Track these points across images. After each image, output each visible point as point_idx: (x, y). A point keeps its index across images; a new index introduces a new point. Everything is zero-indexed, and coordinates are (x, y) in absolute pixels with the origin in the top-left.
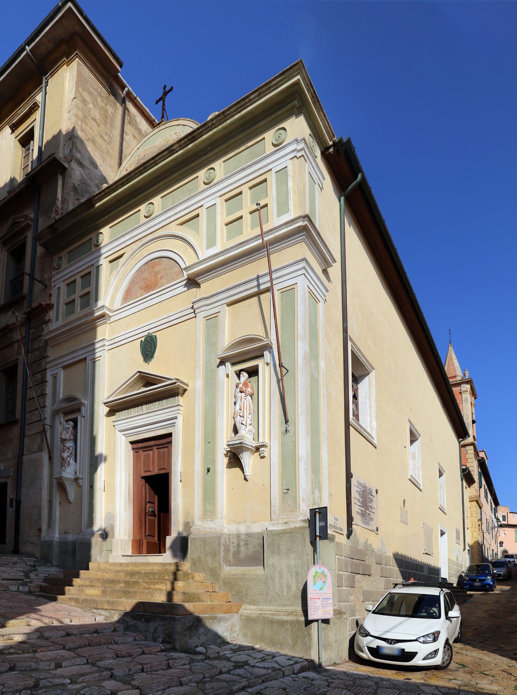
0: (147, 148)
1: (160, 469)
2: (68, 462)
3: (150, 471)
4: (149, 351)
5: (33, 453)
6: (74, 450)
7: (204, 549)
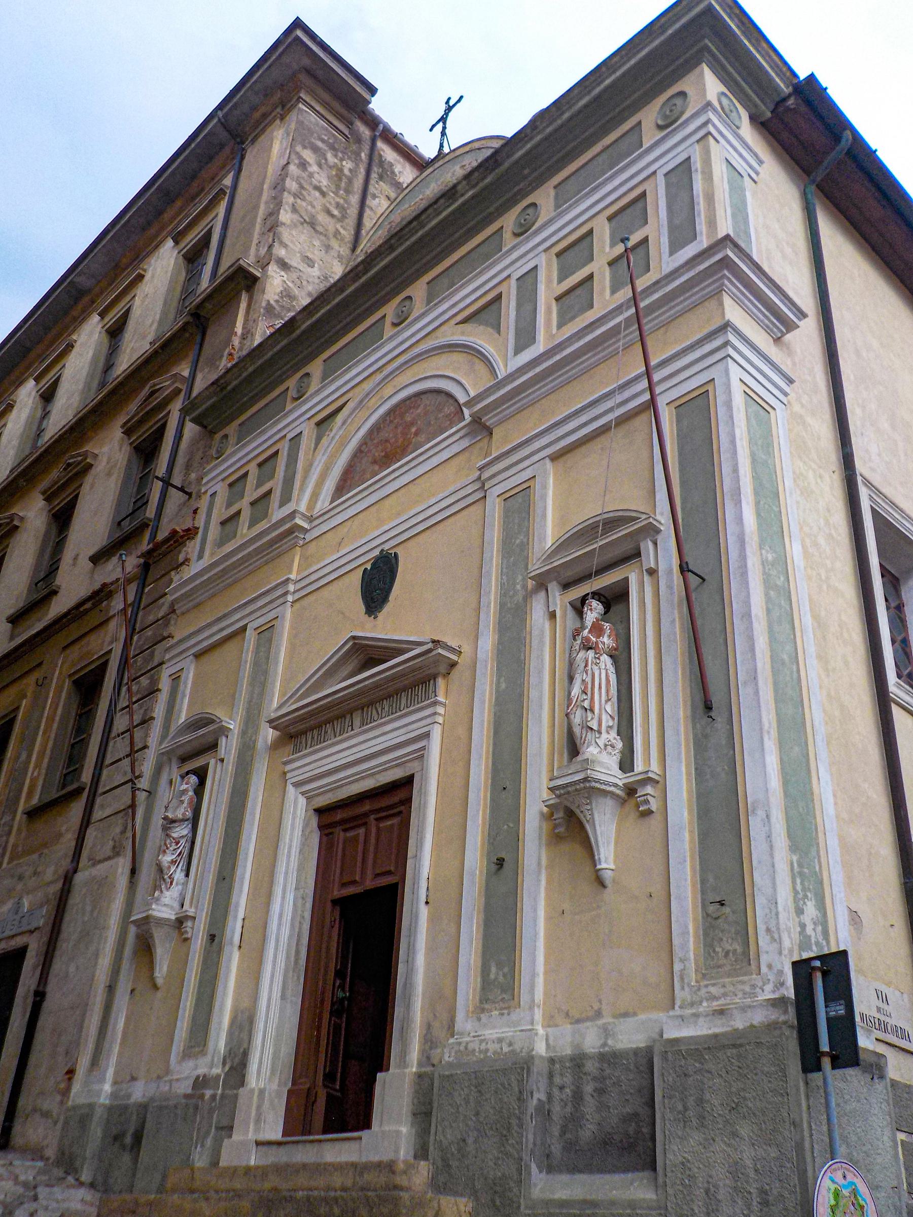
0: (407, 206)
1: (377, 875)
2: (170, 877)
3: (354, 882)
4: (380, 589)
5: (100, 862)
6: (188, 845)
7: (477, 1114)
